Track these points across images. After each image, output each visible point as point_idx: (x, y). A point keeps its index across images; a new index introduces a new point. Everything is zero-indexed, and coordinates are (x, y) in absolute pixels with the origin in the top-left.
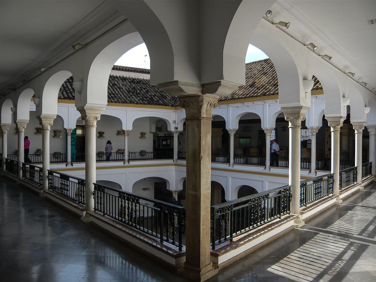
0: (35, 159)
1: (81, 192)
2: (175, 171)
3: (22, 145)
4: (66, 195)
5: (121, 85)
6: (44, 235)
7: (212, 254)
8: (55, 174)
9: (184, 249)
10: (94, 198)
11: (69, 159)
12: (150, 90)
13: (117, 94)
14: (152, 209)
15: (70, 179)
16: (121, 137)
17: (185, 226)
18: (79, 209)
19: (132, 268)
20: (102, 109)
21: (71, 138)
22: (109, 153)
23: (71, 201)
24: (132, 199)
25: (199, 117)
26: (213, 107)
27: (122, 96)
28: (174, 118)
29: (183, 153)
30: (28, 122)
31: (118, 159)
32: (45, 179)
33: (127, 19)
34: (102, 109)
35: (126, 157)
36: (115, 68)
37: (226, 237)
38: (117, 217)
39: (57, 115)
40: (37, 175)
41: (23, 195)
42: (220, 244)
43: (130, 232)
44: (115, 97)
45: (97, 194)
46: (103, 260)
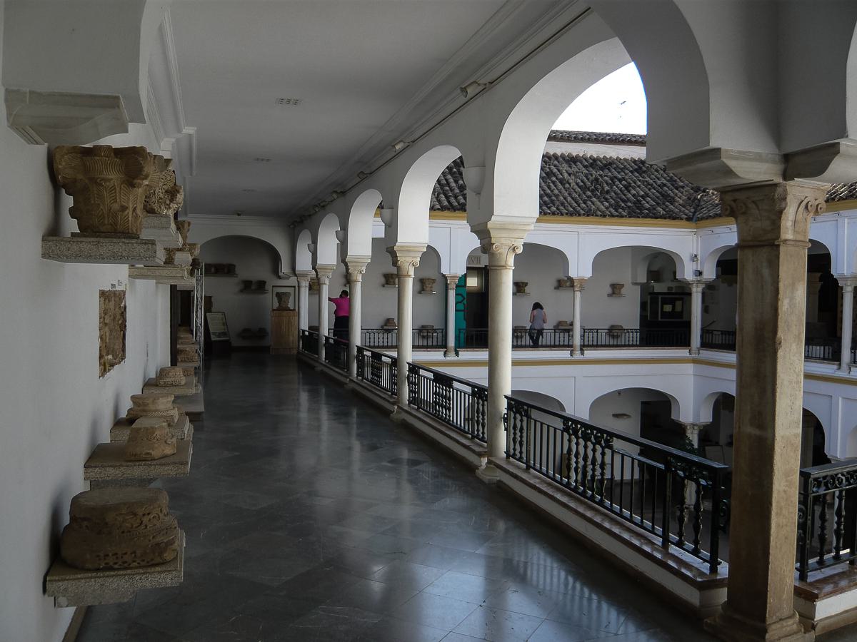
0: (381, 340)
1: (478, 413)
2: (694, 375)
3: (356, 312)
4: (449, 420)
5: (566, 175)
6: (397, 501)
7: (798, 592)
8: (422, 372)
9: (724, 569)
10: (506, 429)
11: (451, 342)
12: (635, 183)
13: (557, 196)
14: (633, 459)
15: (455, 384)
16: (564, 294)
17: (727, 513)
18: (473, 451)
19: (590, 599)
20: (528, 228)
21: (456, 295)
22: (538, 330)
23: (456, 432)
24: (596, 437)
25: (776, 240)
26: (812, 214)
27: (569, 199)
28: (693, 248)
29: (714, 332)
30: (369, 261)
31: (557, 343)
32: (403, 383)
33: (590, 8)
34: (528, 228)
35: (577, 341)
36: (555, 137)
37: (838, 553)
38: (551, 472)
39: (429, 247)
40: (385, 373)
41: (357, 414)
42: (820, 569)
43: (589, 514)
44: (553, 202)
45: (512, 420)
46: (522, 570)
